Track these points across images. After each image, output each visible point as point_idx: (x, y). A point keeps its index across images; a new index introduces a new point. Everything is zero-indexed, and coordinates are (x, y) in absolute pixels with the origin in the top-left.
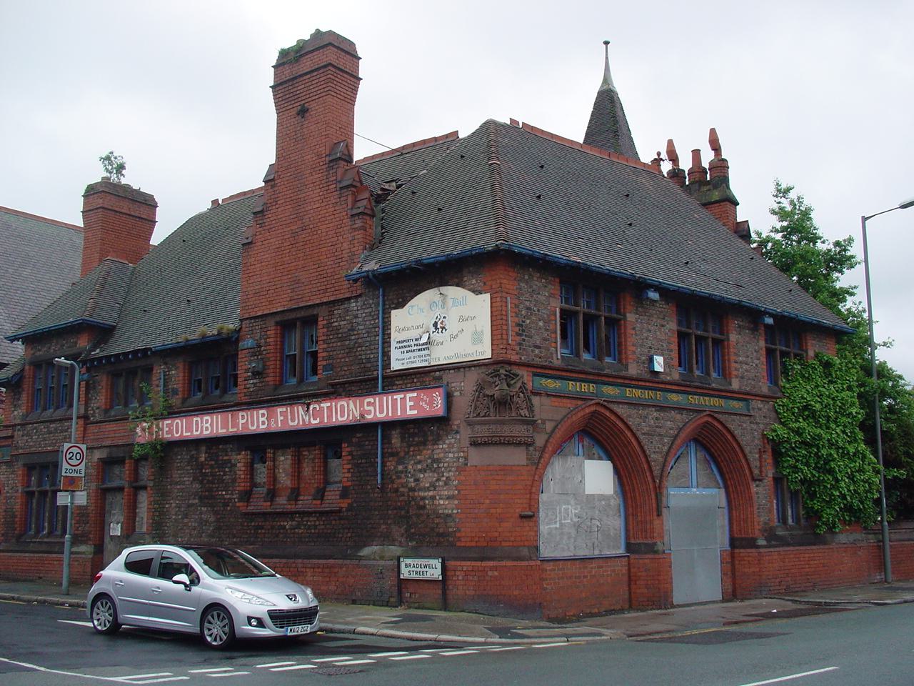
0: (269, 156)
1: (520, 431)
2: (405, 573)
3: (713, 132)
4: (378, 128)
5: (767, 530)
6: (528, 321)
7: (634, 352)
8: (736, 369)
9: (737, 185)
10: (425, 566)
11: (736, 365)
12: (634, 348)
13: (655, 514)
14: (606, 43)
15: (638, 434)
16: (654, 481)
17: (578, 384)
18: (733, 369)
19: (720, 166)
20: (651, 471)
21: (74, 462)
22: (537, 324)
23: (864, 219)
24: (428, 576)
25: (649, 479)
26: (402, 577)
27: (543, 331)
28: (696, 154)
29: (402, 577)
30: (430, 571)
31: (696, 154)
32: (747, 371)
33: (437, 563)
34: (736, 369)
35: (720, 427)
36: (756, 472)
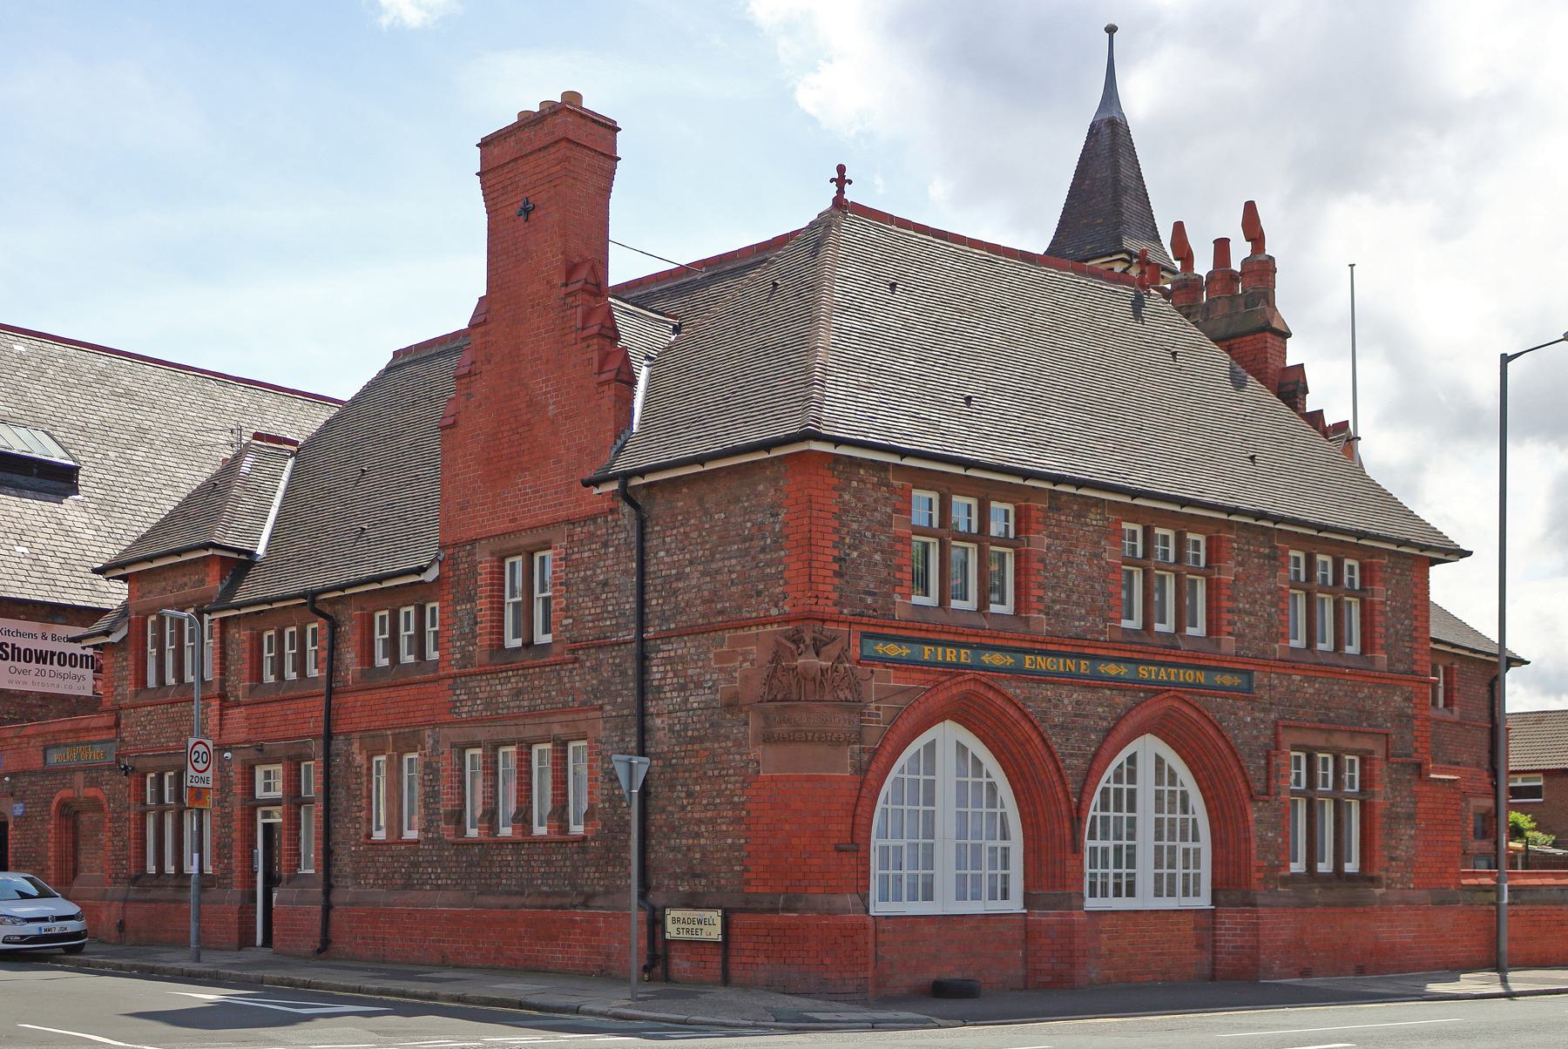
0: (478, 286)
1: (841, 722)
2: (672, 931)
3: (1250, 208)
4: (646, 235)
5: (261, 750)
6: (855, 554)
7: (1040, 599)
8: (1230, 623)
9: (1287, 301)
10: (700, 922)
11: (1230, 616)
12: (1041, 593)
13: (1069, 850)
14: (1111, 30)
15: (1044, 726)
16: (1069, 800)
17: (940, 649)
18: (1225, 622)
19: (1262, 269)
20: (1064, 784)
21: (200, 766)
22: (871, 557)
23: (1505, 359)
24: (703, 936)
25: (1061, 795)
26: (668, 936)
27: (880, 567)
28: (1222, 246)
29: (668, 936)
30: (706, 928)
31: (1222, 246)
32: (1250, 625)
33: (716, 916)
34: (1230, 623)
35: (1194, 715)
36: (1259, 786)
